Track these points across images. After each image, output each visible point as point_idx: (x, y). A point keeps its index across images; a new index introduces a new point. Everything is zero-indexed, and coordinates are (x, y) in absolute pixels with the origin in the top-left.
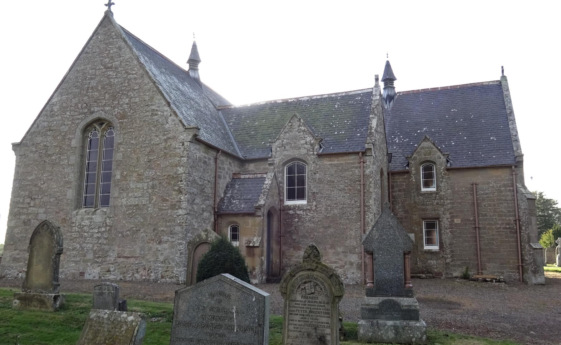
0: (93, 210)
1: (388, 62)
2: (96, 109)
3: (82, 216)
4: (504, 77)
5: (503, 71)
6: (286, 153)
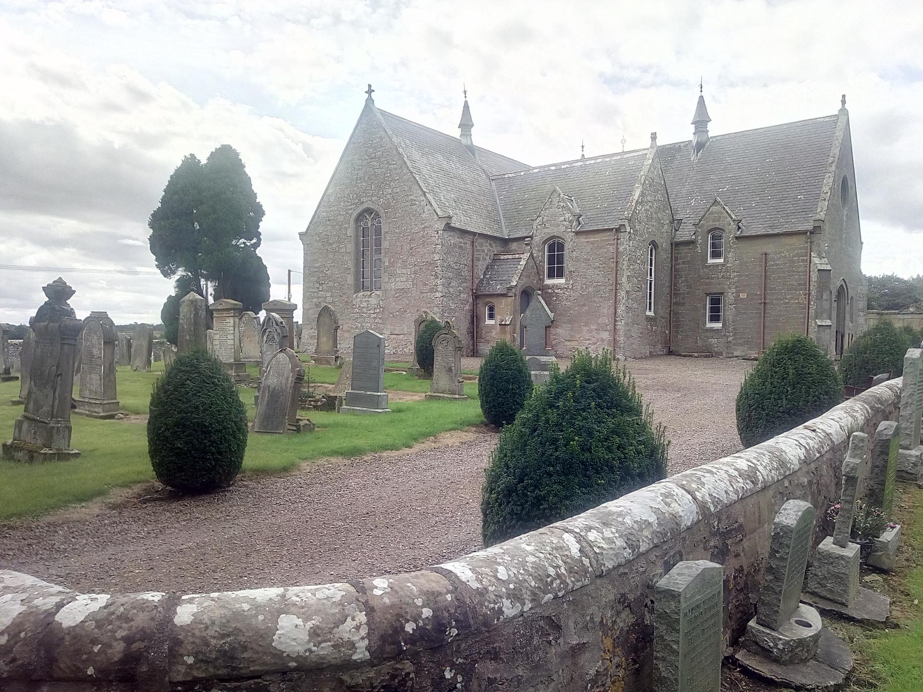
0: (369, 293)
2: (365, 199)
4: (844, 111)
5: (844, 102)
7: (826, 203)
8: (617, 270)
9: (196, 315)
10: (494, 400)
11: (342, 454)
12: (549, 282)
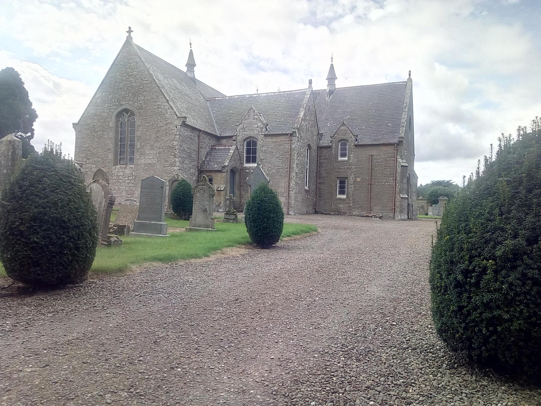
0: (125, 166)
1: (332, 65)
3: (118, 170)
4: (410, 79)
5: (410, 75)
6: (245, 133)
7: (404, 128)
8: (290, 160)
9: (14, 153)
10: (260, 225)
11: (160, 260)
12: (246, 165)
